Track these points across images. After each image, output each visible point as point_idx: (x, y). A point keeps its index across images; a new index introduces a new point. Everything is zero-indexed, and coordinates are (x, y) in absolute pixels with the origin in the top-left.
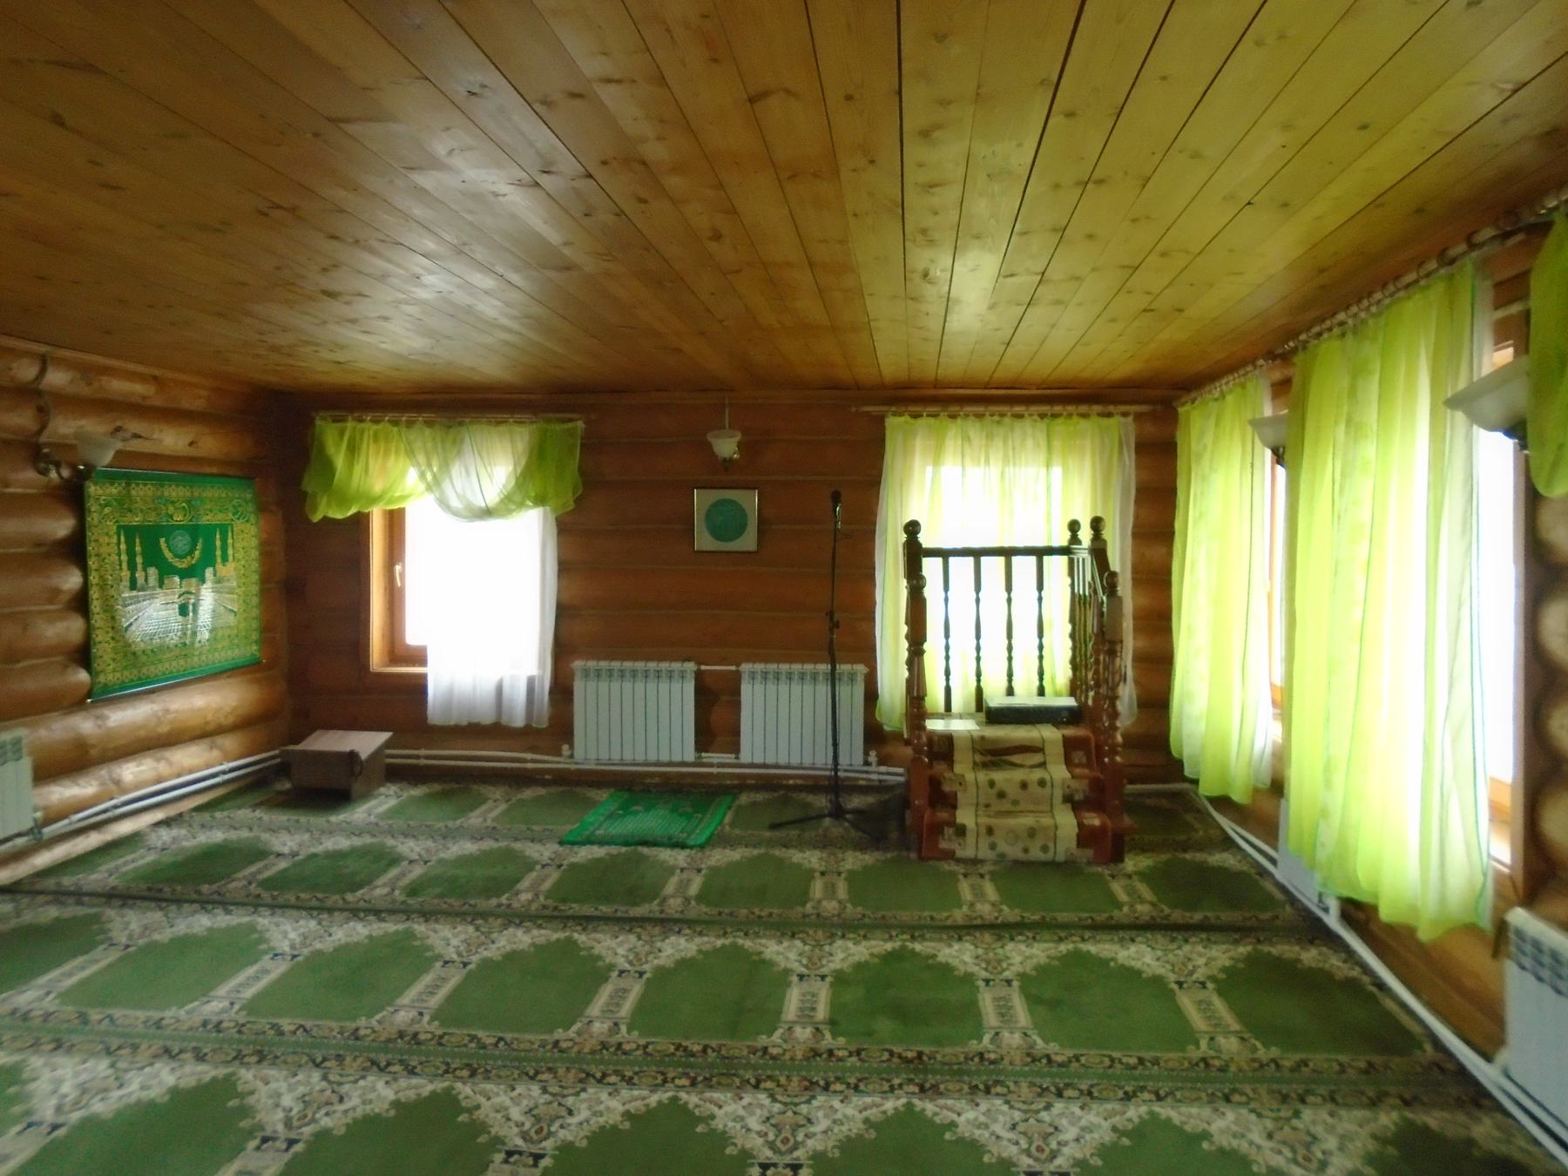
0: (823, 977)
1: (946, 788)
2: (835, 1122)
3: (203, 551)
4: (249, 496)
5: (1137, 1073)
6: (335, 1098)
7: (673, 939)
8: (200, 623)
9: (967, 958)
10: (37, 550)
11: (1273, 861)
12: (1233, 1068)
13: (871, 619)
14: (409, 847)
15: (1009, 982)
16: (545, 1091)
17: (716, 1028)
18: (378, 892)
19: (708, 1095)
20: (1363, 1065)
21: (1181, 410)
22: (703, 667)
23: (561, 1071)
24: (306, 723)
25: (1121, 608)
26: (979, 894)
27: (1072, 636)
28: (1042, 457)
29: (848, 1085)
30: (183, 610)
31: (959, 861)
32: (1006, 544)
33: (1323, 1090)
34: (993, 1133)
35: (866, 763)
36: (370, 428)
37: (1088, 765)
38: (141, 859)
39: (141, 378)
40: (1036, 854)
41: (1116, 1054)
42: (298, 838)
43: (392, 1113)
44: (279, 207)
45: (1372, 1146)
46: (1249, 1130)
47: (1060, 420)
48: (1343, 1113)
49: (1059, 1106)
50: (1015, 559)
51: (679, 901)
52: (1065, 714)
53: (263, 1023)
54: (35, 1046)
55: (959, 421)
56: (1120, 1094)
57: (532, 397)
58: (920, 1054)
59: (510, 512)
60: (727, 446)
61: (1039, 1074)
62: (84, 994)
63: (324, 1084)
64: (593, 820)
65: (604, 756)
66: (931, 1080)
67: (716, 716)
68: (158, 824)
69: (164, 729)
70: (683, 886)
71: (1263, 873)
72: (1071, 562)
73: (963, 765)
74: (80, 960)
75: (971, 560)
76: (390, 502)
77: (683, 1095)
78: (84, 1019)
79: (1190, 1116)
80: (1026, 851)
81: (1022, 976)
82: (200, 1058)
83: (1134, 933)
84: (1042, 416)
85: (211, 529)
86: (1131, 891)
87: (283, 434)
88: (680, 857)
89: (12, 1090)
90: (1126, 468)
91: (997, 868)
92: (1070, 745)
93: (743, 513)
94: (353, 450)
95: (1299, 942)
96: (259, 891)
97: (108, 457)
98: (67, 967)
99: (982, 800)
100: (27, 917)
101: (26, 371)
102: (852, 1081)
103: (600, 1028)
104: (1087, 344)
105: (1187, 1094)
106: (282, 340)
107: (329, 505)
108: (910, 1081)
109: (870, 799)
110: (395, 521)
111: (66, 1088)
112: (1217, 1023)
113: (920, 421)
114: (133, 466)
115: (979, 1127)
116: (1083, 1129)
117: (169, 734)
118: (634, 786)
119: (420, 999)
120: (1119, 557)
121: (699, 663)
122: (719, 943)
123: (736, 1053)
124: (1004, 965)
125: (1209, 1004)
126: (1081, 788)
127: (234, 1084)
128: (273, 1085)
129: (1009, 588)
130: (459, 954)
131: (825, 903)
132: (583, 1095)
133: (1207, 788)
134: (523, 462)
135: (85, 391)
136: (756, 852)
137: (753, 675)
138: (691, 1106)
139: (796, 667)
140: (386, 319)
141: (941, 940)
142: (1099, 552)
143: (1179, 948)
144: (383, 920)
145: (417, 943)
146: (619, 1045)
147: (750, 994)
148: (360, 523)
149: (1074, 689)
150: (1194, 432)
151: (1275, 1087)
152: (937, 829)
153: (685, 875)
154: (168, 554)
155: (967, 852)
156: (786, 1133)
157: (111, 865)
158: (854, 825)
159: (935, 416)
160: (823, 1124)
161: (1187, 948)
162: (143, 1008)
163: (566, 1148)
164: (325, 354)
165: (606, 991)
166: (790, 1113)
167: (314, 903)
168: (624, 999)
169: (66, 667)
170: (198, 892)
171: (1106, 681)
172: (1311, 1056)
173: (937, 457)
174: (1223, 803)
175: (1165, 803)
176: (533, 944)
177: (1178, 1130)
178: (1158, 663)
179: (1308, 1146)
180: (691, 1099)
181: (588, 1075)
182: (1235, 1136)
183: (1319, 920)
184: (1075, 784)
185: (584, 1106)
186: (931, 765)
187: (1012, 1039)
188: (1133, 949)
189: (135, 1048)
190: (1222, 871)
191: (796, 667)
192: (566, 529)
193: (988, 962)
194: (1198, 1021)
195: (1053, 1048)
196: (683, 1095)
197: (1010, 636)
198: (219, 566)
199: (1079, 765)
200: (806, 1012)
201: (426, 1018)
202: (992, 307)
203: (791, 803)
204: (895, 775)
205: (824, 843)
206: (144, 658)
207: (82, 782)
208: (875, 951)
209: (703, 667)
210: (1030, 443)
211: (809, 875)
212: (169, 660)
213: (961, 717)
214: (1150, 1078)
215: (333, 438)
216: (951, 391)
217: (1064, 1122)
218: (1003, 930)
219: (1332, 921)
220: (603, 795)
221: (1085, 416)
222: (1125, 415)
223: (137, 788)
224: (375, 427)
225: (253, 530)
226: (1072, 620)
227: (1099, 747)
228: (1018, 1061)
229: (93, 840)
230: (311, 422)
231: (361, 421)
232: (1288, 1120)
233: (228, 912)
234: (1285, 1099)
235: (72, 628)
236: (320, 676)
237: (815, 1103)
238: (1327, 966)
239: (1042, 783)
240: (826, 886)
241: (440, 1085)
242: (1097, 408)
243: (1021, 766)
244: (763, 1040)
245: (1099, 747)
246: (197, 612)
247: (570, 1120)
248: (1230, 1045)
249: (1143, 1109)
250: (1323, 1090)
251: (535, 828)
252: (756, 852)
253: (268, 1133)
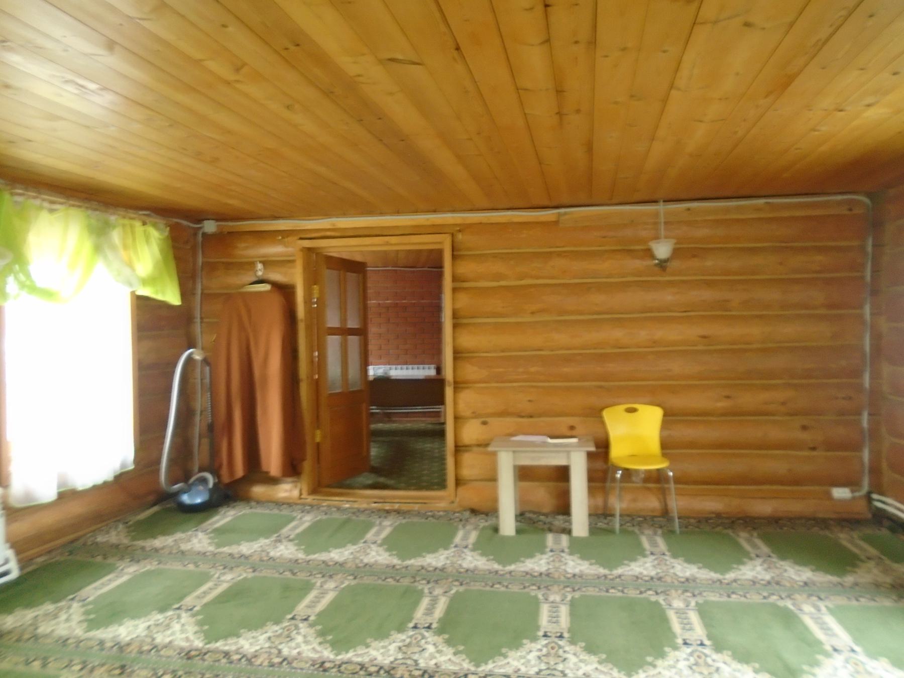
9: (571, 563)
34: (578, 657)
116: (674, 667)
138: (467, 661)
166: (552, 663)
185: (391, 652)
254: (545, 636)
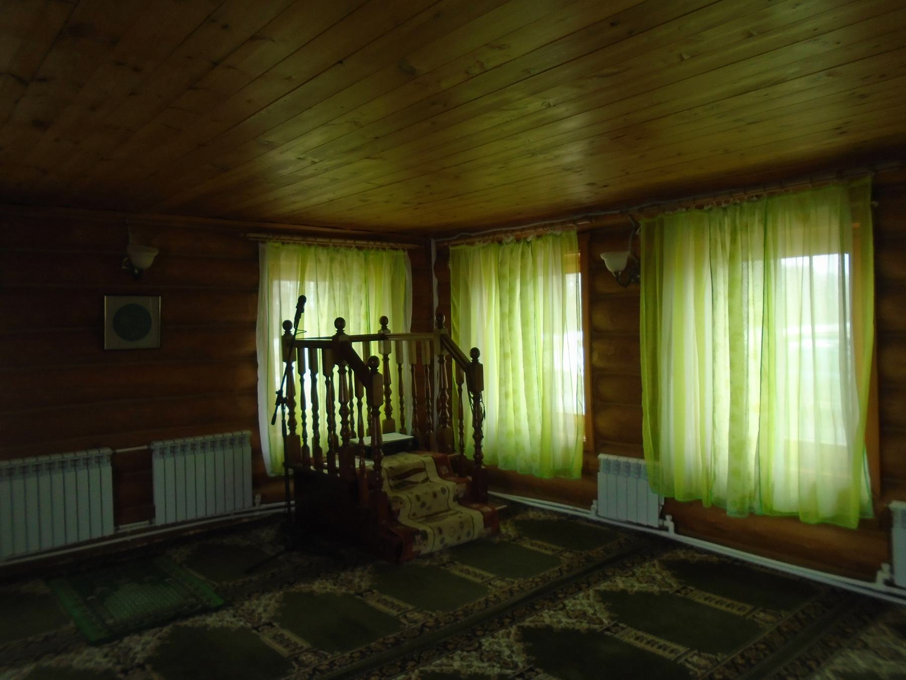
22: (118, 451)
35: (254, 504)
47: (373, 251)
67: (133, 491)
81: (149, 660)
121: (113, 448)
125: (282, 636)
137: (163, 452)
203: (210, 542)
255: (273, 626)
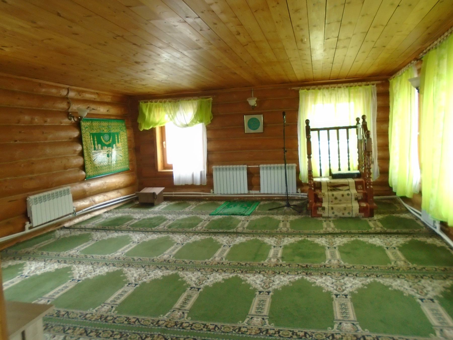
0: (281, 247)
1: (319, 197)
2: (281, 282)
3: (112, 141)
4: (124, 125)
5: (371, 270)
6: (147, 275)
7: (239, 237)
8: (113, 159)
9: (323, 242)
10: (70, 140)
11: (420, 215)
12: (401, 269)
13: (297, 150)
14: (169, 217)
15: (335, 248)
16: (202, 273)
17: (252, 260)
18: (160, 227)
19: (246, 275)
20: (442, 269)
21: (390, 81)
22: (249, 166)
23: (206, 269)
24: (143, 185)
25: (371, 141)
26: (329, 226)
27: (358, 152)
28: (347, 99)
29: (285, 273)
30: (108, 156)
31: (323, 217)
32: (337, 126)
33: (429, 275)
34: (326, 285)
35: (297, 192)
36: (154, 104)
37: (363, 189)
38: (100, 221)
39: (92, 93)
40: (346, 215)
41: (365, 266)
42: (140, 215)
43: (162, 278)
44: (119, 36)
45: (443, 290)
46: (404, 285)
47: (353, 88)
48: (435, 281)
49: (346, 278)
50: (340, 130)
51: (242, 228)
52: (356, 175)
53: (130, 258)
54: (74, 263)
55: (321, 90)
56: (366, 275)
57: (197, 92)
58: (307, 266)
59: (193, 125)
60: (253, 102)
61: (342, 270)
62: (86, 251)
63: (145, 272)
64: (219, 209)
65: (222, 192)
66: (309, 272)
67: (253, 180)
68: (105, 212)
69: (105, 187)
70: (243, 225)
71: (417, 219)
72: (357, 130)
73: (324, 191)
74: (85, 244)
75: (326, 131)
76: (161, 124)
77: (239, 275)
78: (86, 257)
79: (386, 281)
80: (343, 214)
81: (339, 246)
82: (114, 265)
83: (374, 235)
84: (347, 87)
85: (114, 134)
86: (375, 224)
87: (131, 107)
88: (243, 218)
89: (69, 272)
90: (374, 101)
91: (334, 219)
92: (357, 184)
93: (258, 122)
94: (150, 111)
95: (426, 237)
96: (130, 227)
97: (86, 114)
98: (82, 245)
99: (330, 200)
100: (73, 234)
101: (64, 93)
102: (287, 272)
103: (217, 259)
104: (357, 61)
105: (386, 276)
106: (127, 79)
107: (145, 126)
108: (303, 272)
109: (299, 202)
110: (162, 129)
111: (81, 272)
112: (398, 258)
113: (309, 91)
114: (92, 117)
115: (322, 283)
116: (353, 284)
117: (107, 189)
118: (230, 200)
119: (170, 252)
120: (371, 127)
121: (248, 165)
122: (252, 238)
123: (255, 265)
124: (334, 243)
125: (396, 253)
126: (360, 196)
127: (122, 272)
128: (132, 272)
129: (338, 139)
130: (181, 242)
131: (283, 229)
132: (212, 275)
133: (399, 194)
134: (196, 110)
135: (79, 97)
136: (264, 216)
137: (263, 168)
139: (276, 165)
140: (153, 69)
141: (316, 237)
142: (365, 126)
143: (388, 239)
144: (162, 234)
145: (170, 239)
146: (223, 263)
147: (260, 251)
148: (153, 131)
149: (359, 168)
150: (394, 87)
151: (414, 274)
152: (316, 208)
153: (244, 222)
154: (103, 141)
155: (326, 215)
156: (267, 284)
157: (93, 222)
158: (293, 209)
159: (314, 89)
160: (278, 282)
161: (391, 239)
162: (100, 254)
163: (207, 287)
164: (140, 83)
165: (220, 250)
166: (268, 279)
167: (144, 230)
168: (225, 252)
169: (79, 171)
170: (115, 228)
171: (367, 164)
172: (426, 266)
173: (315, 100)
174: (404, 198)
175: (389, 201)
176: (201, 239)
177: (383, 285)
178: (385, 160)
179: (422, 289)
180: (241, 276)
181: (214, 270)
182: (399, 286)
183: (434, 231)
184: (358, 195)
186: (314, 190)
187: (334, 262)
188: (374, 239)
189: (98, 263)
190: (405, 219)
191: (276, 165)
192: (209, 129)
193: (329, 243)
194: (391, 257)
195: (346, 264)
196: (239, 275)
197: (339, 153)
198: (117, 144)
199: (360, 189)
200: (275, 255)
201: (172, 257)
202: (325, 50)
203: (275, 203)
204: (304, 195)
205: (284, 214)
206: (99, 168)
207: (85, 201)
208: (296, 240)
209: (249, 166)
210: (343, 95)
211: (279, 221)
212: (105, 169)
213: (324, 177)
214: (374, 272)
215: (144, 107)
216: (319, 82)
217: (348, 282)
218: (334, 234)
219: (438, 231)
220: (223, 203)
221: (360, 86)
222: (373, 84)
223: (99, 203)
224: (155, 104)
225: (125, 134)
226: (358, 147)
227: (366, 184)
228: (335, 267)
229: (89, 216)
230: (139, 104)
231: (152, 102)
232: (417, 283)
233: (122, 233)
234: (416, 277)
235: (79, 161)
236: (146, 176)
237: (276, 277)
238: (435, 243)
239: (348, 195)
240: (284, 224)
241: (174, 272)
242: (365, 83)
243: (342, 190)
244: (262, 262)
245: (366, 184)
246: (112, 156)
247: (208, 280)
248: (401, 264)
249: (372, 280)
250: (429, 275)
251: (203, 211)
252: (264, 216)
253: (130, 282)
254: (346, 296)
255: (433, 302)
